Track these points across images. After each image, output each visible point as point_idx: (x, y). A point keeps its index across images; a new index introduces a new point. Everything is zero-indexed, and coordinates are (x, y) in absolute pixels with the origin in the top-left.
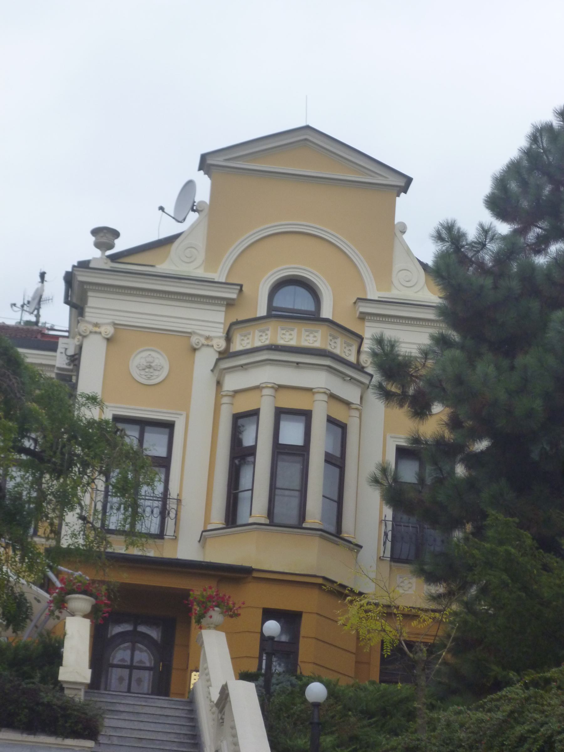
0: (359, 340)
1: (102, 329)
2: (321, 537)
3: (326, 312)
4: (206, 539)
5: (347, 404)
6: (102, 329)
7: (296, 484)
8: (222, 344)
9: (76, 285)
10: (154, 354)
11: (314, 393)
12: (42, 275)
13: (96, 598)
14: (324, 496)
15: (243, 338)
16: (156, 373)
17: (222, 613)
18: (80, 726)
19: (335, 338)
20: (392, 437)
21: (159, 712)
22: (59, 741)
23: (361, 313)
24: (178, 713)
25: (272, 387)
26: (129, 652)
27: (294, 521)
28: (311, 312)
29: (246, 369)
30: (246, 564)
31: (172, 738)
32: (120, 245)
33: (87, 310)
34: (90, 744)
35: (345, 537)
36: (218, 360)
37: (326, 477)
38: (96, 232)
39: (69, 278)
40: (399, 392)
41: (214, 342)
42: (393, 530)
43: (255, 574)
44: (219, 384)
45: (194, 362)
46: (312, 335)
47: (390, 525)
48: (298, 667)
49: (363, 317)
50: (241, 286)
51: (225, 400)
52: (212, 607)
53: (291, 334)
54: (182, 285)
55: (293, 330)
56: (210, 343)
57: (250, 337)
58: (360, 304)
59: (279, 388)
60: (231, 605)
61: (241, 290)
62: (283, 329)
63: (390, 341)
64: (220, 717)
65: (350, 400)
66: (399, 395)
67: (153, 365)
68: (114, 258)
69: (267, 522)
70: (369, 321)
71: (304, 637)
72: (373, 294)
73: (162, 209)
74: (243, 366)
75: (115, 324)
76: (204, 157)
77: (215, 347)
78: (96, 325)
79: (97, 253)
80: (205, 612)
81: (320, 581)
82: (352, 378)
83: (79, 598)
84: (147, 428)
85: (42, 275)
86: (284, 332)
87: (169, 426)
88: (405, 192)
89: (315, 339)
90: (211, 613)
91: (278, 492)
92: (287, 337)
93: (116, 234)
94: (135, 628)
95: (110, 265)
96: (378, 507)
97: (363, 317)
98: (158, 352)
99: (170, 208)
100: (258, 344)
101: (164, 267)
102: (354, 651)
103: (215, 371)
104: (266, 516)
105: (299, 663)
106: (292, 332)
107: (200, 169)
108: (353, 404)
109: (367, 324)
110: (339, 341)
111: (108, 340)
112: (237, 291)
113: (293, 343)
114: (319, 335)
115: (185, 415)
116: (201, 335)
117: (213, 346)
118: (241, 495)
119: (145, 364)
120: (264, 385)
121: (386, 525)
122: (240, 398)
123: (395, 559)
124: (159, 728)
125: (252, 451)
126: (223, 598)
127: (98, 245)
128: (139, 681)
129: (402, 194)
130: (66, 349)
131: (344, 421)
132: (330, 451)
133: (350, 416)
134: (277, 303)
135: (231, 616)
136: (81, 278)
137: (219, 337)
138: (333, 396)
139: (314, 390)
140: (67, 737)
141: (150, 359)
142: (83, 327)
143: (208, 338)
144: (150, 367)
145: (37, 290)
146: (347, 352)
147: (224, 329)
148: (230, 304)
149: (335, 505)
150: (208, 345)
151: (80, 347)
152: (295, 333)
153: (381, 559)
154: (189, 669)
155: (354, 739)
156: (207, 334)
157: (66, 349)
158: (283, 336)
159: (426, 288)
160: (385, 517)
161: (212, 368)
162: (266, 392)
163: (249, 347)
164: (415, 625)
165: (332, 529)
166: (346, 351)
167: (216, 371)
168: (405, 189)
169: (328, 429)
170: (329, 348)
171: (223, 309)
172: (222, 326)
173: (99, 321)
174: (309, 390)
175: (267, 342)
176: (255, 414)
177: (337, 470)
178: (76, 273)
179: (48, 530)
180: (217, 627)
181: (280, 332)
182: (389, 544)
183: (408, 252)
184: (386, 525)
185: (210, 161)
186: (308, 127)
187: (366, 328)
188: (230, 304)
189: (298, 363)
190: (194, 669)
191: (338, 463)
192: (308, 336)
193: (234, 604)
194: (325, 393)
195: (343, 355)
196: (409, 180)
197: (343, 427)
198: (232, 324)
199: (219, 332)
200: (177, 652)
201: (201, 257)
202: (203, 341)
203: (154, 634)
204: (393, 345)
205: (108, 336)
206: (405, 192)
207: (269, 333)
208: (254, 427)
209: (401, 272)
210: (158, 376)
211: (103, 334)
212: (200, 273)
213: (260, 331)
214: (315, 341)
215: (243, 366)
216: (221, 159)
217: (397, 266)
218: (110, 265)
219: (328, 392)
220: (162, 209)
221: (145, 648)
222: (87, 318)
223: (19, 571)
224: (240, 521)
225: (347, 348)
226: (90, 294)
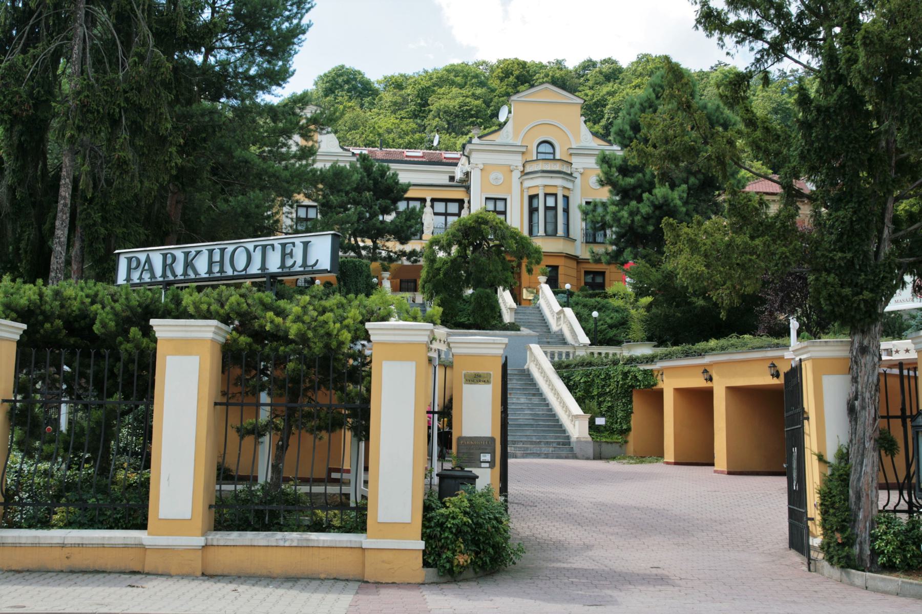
5: (569, 189)
8: (522, 169)
35: (504, 300)
49: (571, 154)
59: (545, 186)
74: (531, 178)
87: (505, 200)
97: (571, 154)
113: (545, 169)
125: (537, 209)
138: (564, 188)
164: (891, 507)
174: (556, 186)
188: (523, 153)
201: (511, 135)
212: (511, 142)
215: (531, 178)
223: (177, 301)
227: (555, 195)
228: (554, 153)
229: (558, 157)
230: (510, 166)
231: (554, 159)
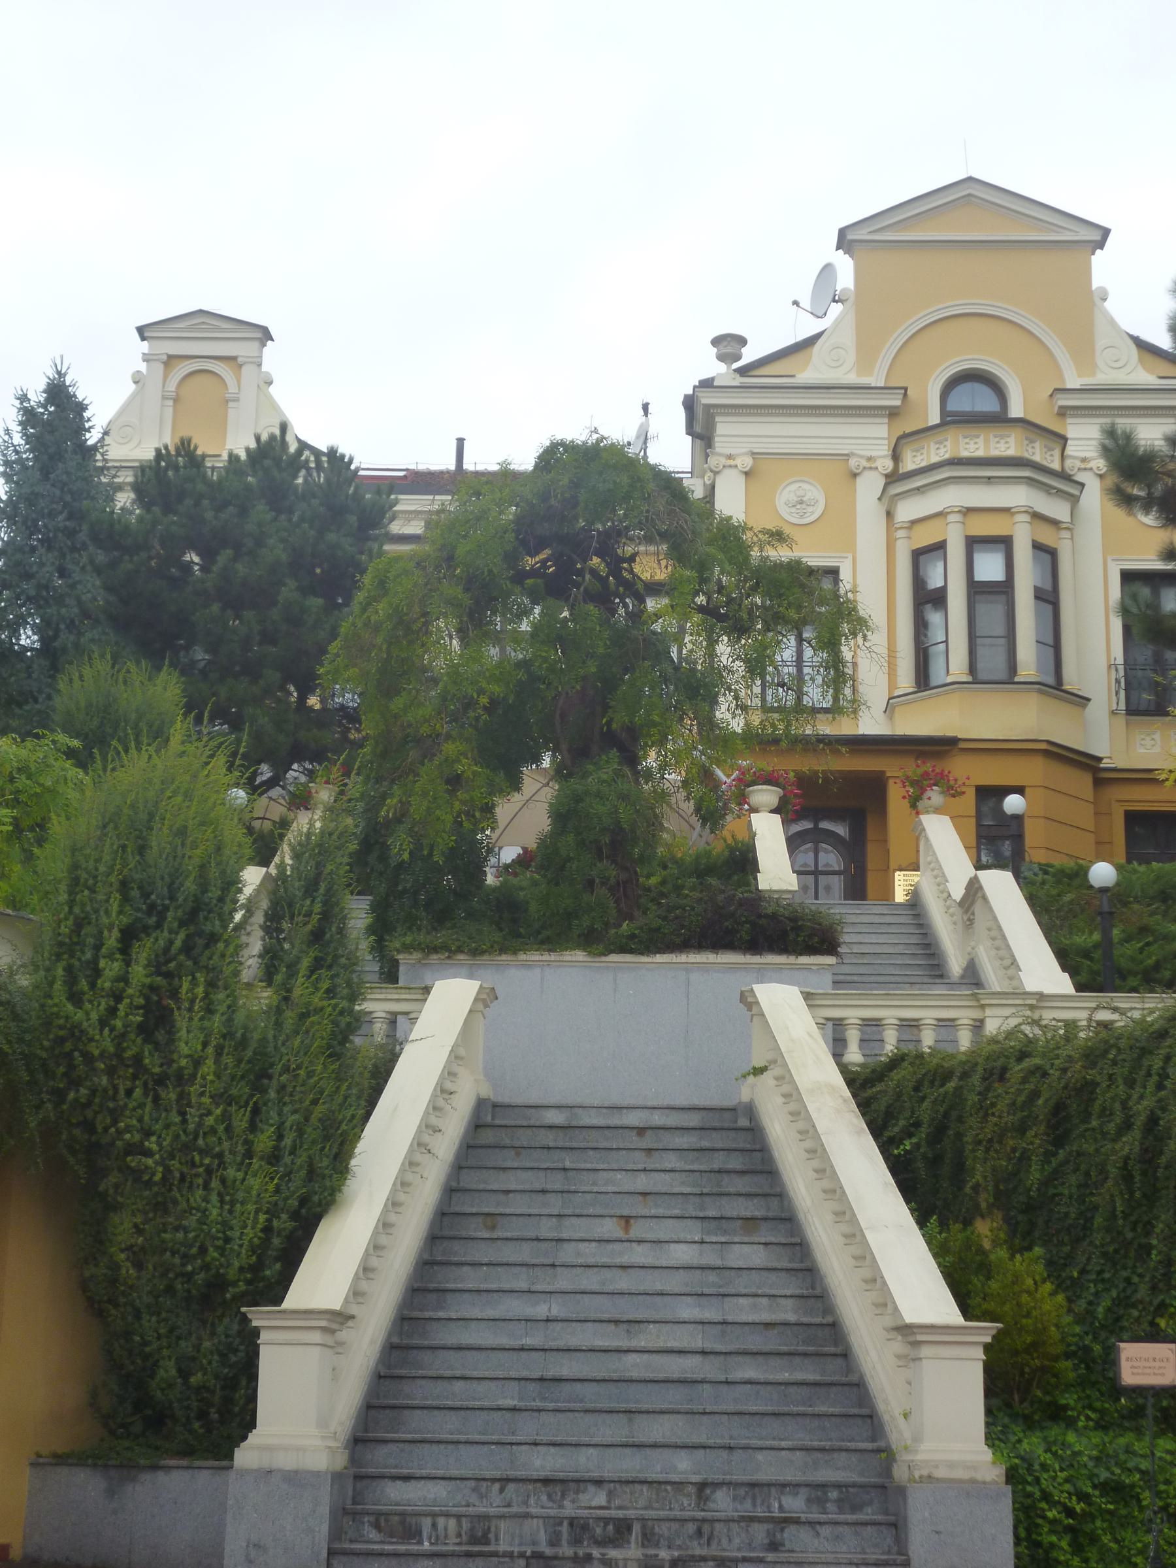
0: (1062, 442)
1: (738, 462)
2: (1040, 692)
3: (1016, 410)
4: (894, 708)
5: (1055, 523)
6: (738, 462)
7: (1000, 630)
8: (889, 465)
9: (699, 411)
10: (805, 486)
11: (1013, 514)
12: (645, 408)
13: (784, 789)
16: (810, 509)
17: (942, 793)
18: (816, 939)
19: (1032, 441)
21: (877, 920)
22: (792, 959)
23: (1061, 407)
24: (901, 920)
25: (959, 512)
26: (811, 855)
27: (1002, 675)
29: (923, 493)
30: (950, 733)
31: (900, 949)
32: (749, 355)
33: (717, 439)
34: (830, 960)
36: (886, 485)
37: (1038, 614)
38: (716, 342)
39: (689, 404)
40: (1142, 494)
42: (1126, 676)
43: (962, 745)
44: (889, 514)
46: (1003, 441)
47: (1121, 669)
49: (1063, 412)
50: (906, 389)
51: (901, 534)
52: (930, 786)
55: (978, 437)
57: (925, 451)
58: (1058, 396)
59: (969, 511)
60: (952, 783)
61: (905, 395)
62: (965, 437)
63: (1124, 433)
64: (965, 918)
66: (1144, 498)
68: (743, 371)
69: (970, 679)
72: (1073, 382)
73: (796, 303)
75: (753, 453)
76: (842, 233)
78: (730, 457)
79: (721, 368)
80: (922, 794)
81: (1044, 746)
82: (1059, 491)
83: (761, 790)
85: (645, 408)
86: (967, 440)
88: (1102, 248)
90: (929, 793)
91: (979, 641)
92: (972, 447)
93: (742, 341)
94: (816, 825)
95: (739, 380)
97: (1063, 412)
99: (806, 303)
100: (935, 459)
101: (806, 376)
102: (1092, 829)
107: (838, 249)
109: (1069, 420)
110: (1037, 445)
111: (746, 474)
113: (980, 453)
114: (1012, 440)
115: (850, 556)
116: (861, 457)
118: (932, 650)
119: (795, 499)
121: (1117, 670)
122: (919, 529)
123: (1133, 711)
124: (882, 938)
126: (941, 774)
127: (721, 358)
128: (828, 888)
129: (1098, 251)
131: (1053, 545)
132: (1039, 585)
134: (952, 406)
135: (954, 796)
136: (705, 401)
138: (1037, 516)
140: (801, 954)
141: (800, 493)
142: (713, 461)
143: (869, 459)
144: (801, 502)
145: (641, 426)
146: (1049, 458)
147: (889, 445)
148: (893, 414)
149: (1051, 651)
150: (871, 468)
151: (713, 487)
152: (981, 441)
153: (1113, 713)
154: (892, 868)
155: (1144, 930)
156: (868, 454)
159: (1140, 368)
162: (951, 518)
163: (924, 464)
165: (1051, 680)
166: (1047, 456)
167: (886, 500)
168: (1101, 244)
169: (1035, 558)
170: (1026, 455)
171: (886, 420)
172: (886, 442)
173: (733, 451)
174: (1006, 510)
175: (947, 456)
177: (1049, 607)
178: (700, 395)
179: (733, 706)
180: (938, 810)
181: (962, 441)
182: (1122, 694)
183: (1113, 323)
184: (1117, 670)
185: (850, 237)
186: (970, 179)
188: (893, 414)
189: (989, 478)
191: (1051, 599)
193: (956, 780)
194: (1026, 512)
195: (1045, 463)
196: (1106, 232)
197: (1052, 553)
198: (899, 439)
199: (882, 451)
200: (872, 851)
201: (851, 358)
202: (864, 463)
203: (841, 830)
204: (1128, 437)
206: (1102, 248)
207: (948, 443)
208: (940, 565)
210: (813, 513)
212: (852, 378)
215: (918, 489)
216: (865, 231)
217: (1100, 343)
218: (739, 380)
220: (796, 303)
221: (831, 848)
222: (718, 450)
224: (934, 682)
226: (718, 419)
227: (1005, 543)
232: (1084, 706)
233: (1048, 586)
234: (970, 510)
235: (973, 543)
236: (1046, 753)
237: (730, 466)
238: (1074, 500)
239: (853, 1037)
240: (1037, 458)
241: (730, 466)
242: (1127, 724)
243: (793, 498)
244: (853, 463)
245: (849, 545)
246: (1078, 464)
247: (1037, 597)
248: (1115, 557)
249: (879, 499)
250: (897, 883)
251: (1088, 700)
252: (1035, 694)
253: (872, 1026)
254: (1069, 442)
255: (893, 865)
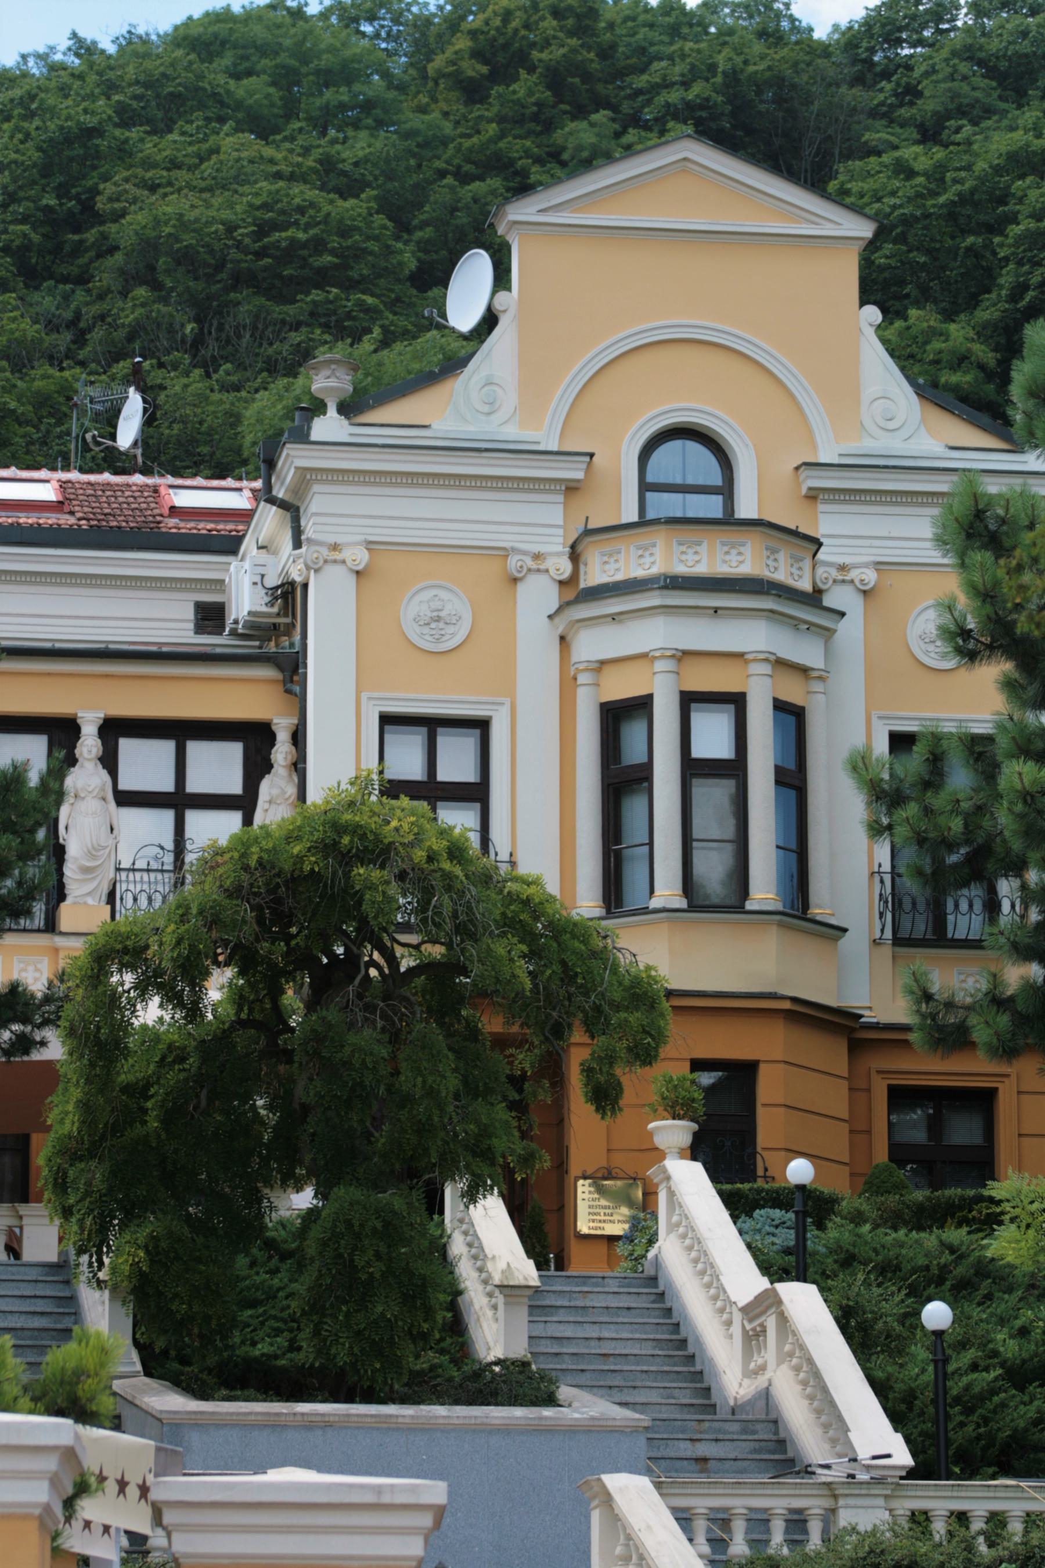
5: (804, 671)
6: (347, 554)
8: (565, 569)
10: (444, 594)
11: (747, 662)
14: (778, 847)
15: (606, 559)
16: (450, 629)
19: (774, 551)
20: (880, 718)
25: (673, 656)
28: (717, 487)
29: (620, 622)
37: (780, 803)
41: (550, 564)
45: (515, 603)
46: (734, 552)
47: (888, 879)
48: (759, 1157)
49: (813, 496)
53: (696, 553)
54: (484, 461)
55: (699, 544)
56: (542, 567)
59: (684, 656)
61: (589, 464)
62: (680, 544)
65: (809, 663)
67: (442, 614)
70: (825, 501)
71: (764, 1105)
74: (614, 617)
77: (552, 572)
81: (787, 1005)
82: (811, 624)
84: (440, 730)
86: (683, 548)
87: (482, 726)
89: (740, 558)
96: (865, 847)
97: (813, 496)
98: (451, 591)
102: (846, 1117)
103: (557, 620)
104: (680, 892)
105: (759, 1149)
106: (698, 548)
108: (813, 669)
109: (821, 507)
110: (781, 556)
112: (584, 466)
113: (702, 569)
114: (748, 550)
115: (507, 706)
116: (525, 553)
117: (547, 571)
120: (657, 654)
121: (882, 882)
130: (263, 576)
133: (808, 692)
137: (558, 554)
138: (781, 664)
139: (747, 657)
141: (436, 604)
144: (438, 619)
146: (796, 572)
149: (794, 857)
152: (703, 549)
156: (535, 548)
157: (263, 576)
158: (684, 557)
159: (923, 429)
160: (880, 866)
161: (552, 612)
162: (660, 666)
163: (620, 577)
171: (561, 498)
173: (339, 539)
174: (740, 656)
176: (642, 705)
177: (792, 794)
184: (882, 882)
187: (821, 516)
188: (571, 488)
190: (580, 1174)
191: (796, 783)
192: (727, 553)
194: (766, 660)
201: (509, 400)
202: (530, 563)
205: (360, 568)
209: (876, 403)
211: (349, 563)
212: (512, 432)
213: (639, 548)
214: (741, 562)
215: (614, 617)
219: (772, 658)
225: (796, 566)
227: (737, 702)
228: (727, 490)
229: (746, 508)
230: (504, 553)
231: (729, 520)
232: (837, 939)
233: (791, 765)
234: (686, 653)
235: (689, 700)
236: (789, 1015)
237: (335, 561)
238: (828, 633)
239: (739, 1527)
240: (781, 576)
241: (335, 561)
242: (894, 957)
243: (425, 611)
244: (513, 562)
245: (508, 687)
246: (834, 573)
247: (778, 782)
248: (883, 713)
249: (550, 617)
250: (580, 1195)
251: (845, 930)
252: (774, 930)
253: (759, 1521)
254: (822, 549)
255: (574, 1169)
